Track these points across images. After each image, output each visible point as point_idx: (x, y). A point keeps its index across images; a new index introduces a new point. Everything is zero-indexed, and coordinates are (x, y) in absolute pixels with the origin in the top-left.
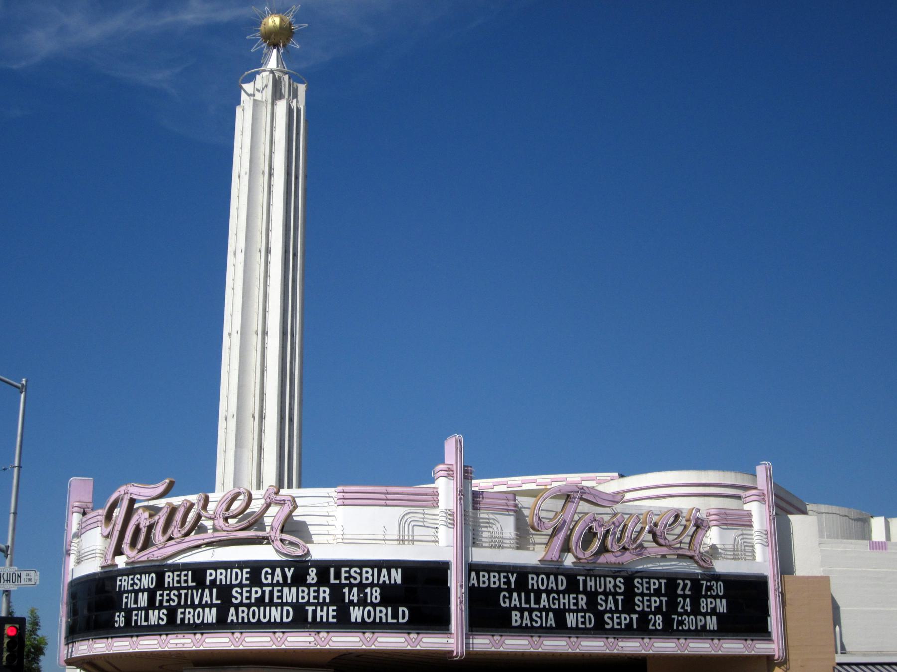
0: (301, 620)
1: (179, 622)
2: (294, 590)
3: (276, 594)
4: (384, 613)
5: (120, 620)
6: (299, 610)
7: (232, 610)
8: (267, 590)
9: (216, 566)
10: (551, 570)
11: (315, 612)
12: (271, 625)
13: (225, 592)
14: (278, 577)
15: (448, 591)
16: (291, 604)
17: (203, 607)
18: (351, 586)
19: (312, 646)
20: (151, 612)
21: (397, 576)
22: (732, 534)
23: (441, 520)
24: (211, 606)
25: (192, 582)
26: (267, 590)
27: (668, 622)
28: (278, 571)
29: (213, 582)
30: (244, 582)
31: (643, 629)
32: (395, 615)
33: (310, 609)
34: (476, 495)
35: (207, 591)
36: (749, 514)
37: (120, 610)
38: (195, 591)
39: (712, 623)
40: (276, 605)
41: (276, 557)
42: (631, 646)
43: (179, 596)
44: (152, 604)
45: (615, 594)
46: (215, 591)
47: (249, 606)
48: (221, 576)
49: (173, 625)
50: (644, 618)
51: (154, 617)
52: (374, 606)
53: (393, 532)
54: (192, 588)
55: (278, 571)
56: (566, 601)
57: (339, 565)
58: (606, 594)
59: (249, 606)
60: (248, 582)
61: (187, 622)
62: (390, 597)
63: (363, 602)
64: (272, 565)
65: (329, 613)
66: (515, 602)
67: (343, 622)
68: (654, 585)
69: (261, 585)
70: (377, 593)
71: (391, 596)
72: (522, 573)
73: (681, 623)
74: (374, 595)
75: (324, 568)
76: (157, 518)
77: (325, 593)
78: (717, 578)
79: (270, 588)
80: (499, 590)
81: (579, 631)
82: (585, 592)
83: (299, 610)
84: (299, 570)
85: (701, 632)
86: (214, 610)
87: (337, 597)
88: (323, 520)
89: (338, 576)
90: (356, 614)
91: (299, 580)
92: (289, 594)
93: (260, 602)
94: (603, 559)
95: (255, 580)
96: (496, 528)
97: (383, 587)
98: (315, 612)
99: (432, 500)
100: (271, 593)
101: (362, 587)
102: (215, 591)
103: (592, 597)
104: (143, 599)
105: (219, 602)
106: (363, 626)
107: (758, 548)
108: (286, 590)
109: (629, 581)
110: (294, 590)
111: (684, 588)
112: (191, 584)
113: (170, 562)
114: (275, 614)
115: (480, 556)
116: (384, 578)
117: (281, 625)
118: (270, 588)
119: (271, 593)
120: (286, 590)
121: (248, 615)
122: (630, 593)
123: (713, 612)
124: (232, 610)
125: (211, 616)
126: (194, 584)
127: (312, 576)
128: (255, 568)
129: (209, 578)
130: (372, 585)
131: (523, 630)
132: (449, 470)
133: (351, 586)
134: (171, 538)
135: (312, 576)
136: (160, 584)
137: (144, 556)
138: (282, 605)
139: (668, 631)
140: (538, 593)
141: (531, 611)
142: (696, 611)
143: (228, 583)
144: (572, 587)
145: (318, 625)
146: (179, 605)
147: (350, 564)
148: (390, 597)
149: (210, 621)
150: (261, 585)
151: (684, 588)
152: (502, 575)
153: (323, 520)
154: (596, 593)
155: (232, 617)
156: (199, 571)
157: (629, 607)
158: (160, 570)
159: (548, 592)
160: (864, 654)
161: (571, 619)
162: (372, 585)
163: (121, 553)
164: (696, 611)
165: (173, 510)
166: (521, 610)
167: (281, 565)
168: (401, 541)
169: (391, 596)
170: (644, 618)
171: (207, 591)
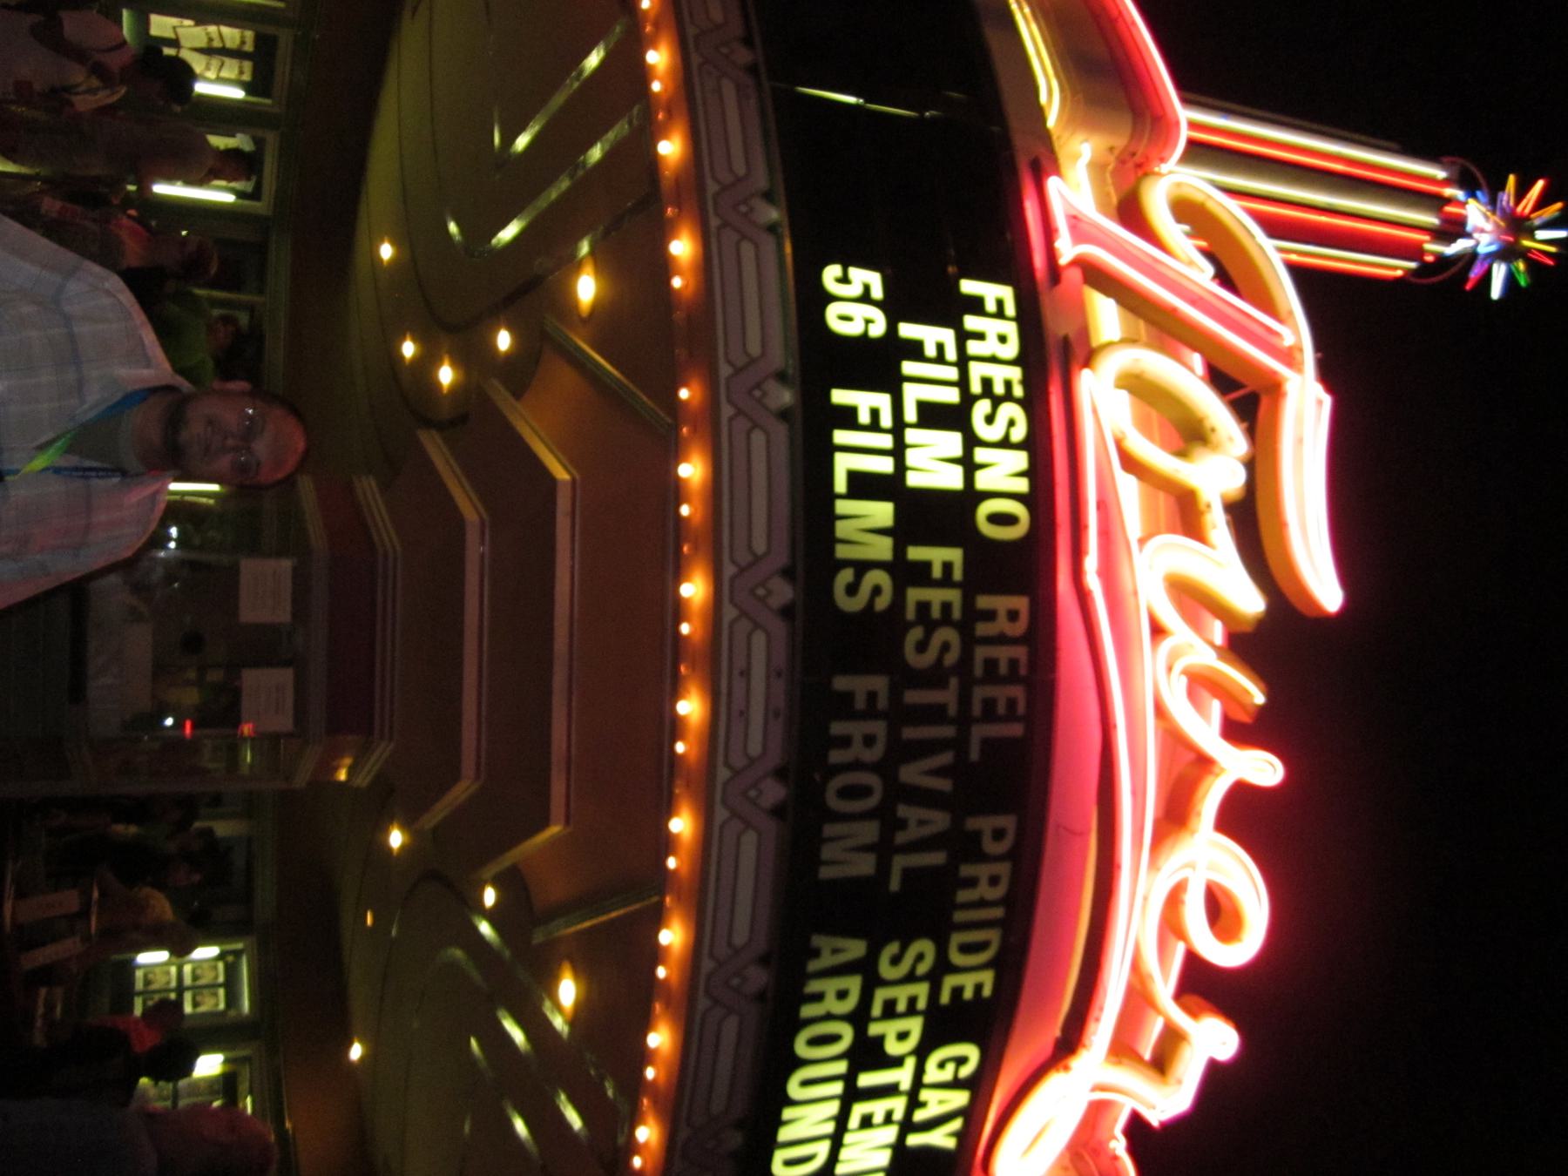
1: (840, 396)
17: (886, 817)
18: (973, 615)
24: (884, 850)
25: (987, 743)
30: (950, 982)
37: (895, 308)
38: (946, 758)
46: (937, 858)
54: (959, 745)
60: (945, 998)
61: (837, 728)
79: (952, 710)
102: (937, 858)
105: (895, 884)
112: (979, 732)
118: (952, 710)
121: (857, 766)
126: (974, 755)
133: (973, 615)
143: (959, 916)
146: (906, 677)
149: (842, 529)
152: (1020, 653)
171: (940, 821)
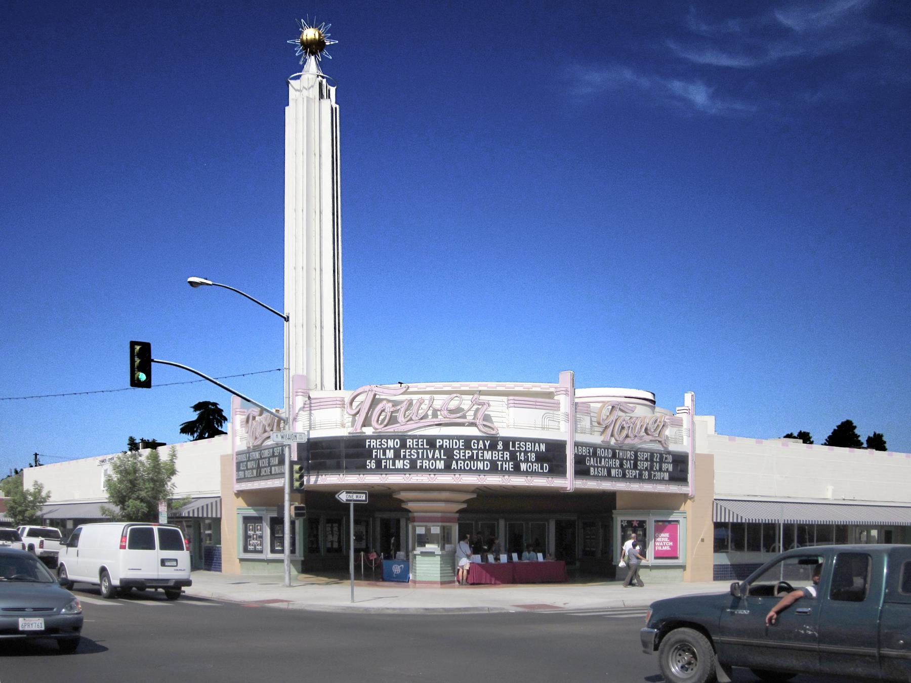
0: (494, 468)
2: (490, 452)
3: (480, 455)
4: (536, 467)
5: (371, 464)
6: (494, 464)
7: (454, 462)
8: (475, 452)
9: (443, 437)
10: (606, 447)
11: (502, 465)
12: (478, 471)
13: (449, 454)
14: (481, 445)
15: (566, 456)
16: (488, 460)
18: (520, 452)
19: (501, 483)
20: (397, 461)
21: (543, 447)
22: (675, 429)
23: (562, 417)
24: (440, 459)
26: (475, 452)
27: (650, 475)
28: (481, 442)
29: (441, 447)
31: (639, 478)
32: (542, 468)
33: (499, 463)
34: (576, 403)
35: (437, 451)
36: (681, 420)
39: (666, 476)
40: (481, 461)
41: (479, 434)
42: (648, 488)
43: (418, 453)
44: (397, 456)
45: (630, 460)
47: (464, 461)
48: (446, 443)
49: (413, 468)
50: (641, 475)
51: (399, 464)
52: (532, 463)
53: (539, 424)
55: (481, 442)
56: (611, 463)
57: (514, 440)
58: (627, 460)
59: (464, 461)
62: (540, 458)
63: (527, 460)
64: (478, 439)
65: (509, 466)
66: (592, 463)
67: (517, 470)
68: (646, 455)
69: (471, 449)
70: (533, 455)
71: (541, 458)
72: (595, 447)
73: (655, 476)
74: (532, 457)
75: (507, 442)
76: (399, 407)
77: (507, 455)
78: (669, 453)
80: (586, 456)
81: (616, 479)
82: (619, 458)
83: (494, 464)
84: (493, 443)
85: (662, 481)
86: (442, 462)
87: (513, 457)
88: (500, 414)
89: (514, 446)
90: (523, 466)
91: (493, 447)
92: (488, 455)
93: (471, 458)
94: (628, 441)
95: (467, 446)
96: (583, 423)
97: (536, 453)
98: (502, 465)
99: (556, 407)
100: (477, 454)
101: (526, 452)
103: (621, 460)
104: (390, 454)
106: (527, 473)
107: (685, 438)
108: (485, 452)
109: (652, 455)
110: (490, 452)
111: (656, 458)
113: (409, 433)
114: (480, 465)
115: (581, 438)
116: (537, 448)
117: (440, 471)
119: (477, 454)
120: (485, 452)
122: (636, 459)
123: (667, 471)
124: (454, 462)
125: (441, 465)
127: (500, 446)
128: (468, 441)
129: (438, 445)
130: (531, 452)
131: (596, 477)
132: (566, 391)
134: (411, 419)
135: (500, 446)
136: (404, 445)
137: (391, 429)
138: (484, 460)
139: (650, 479)
140: (601, 458)
141: (598, 467)
142: (660, 470)
144: (614, 456)
145: (504, 472)
147: (520, 440)
148: (540, 458)
150: (471, 449)
151: (656, 458)
153: (500, 414)
154: (623, 459)
155: (454, 465)
156: (431, 442)
157: (635, 467)
158: (403, 439)
159: (605, 458)
160: (725, 495)
161: (613, 472)
162: (531, 452)
163: (370, 425)
164: (660, 470)
165: (410, 403)
166: (594, 467)
167: (483, 439)
168: (543, 428)
169: (541, 458)
170: (641, 475)
171: (437, 451)
